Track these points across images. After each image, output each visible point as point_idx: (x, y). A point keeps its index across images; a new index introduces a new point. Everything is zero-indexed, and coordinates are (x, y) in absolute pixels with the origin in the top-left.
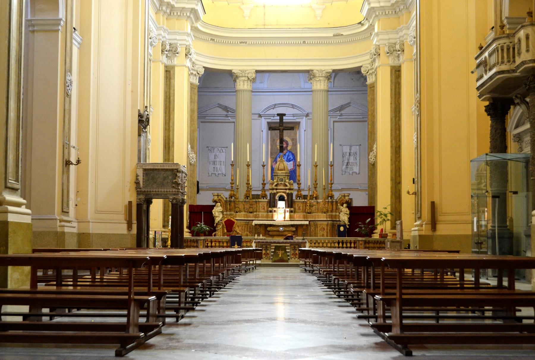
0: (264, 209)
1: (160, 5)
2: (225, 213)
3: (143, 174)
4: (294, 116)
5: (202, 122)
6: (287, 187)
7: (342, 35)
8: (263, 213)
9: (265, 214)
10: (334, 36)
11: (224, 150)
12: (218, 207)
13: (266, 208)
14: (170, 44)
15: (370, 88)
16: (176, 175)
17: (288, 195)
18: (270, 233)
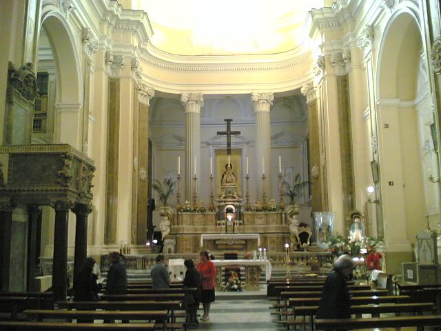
1: (104, 15)
3: (10, 161)
6: (235, 200)
8: (211, 226)
13: (214, 222)
14: (115, 57)
15: (311, 106)
16: (64, 162)
18: (219, 247)
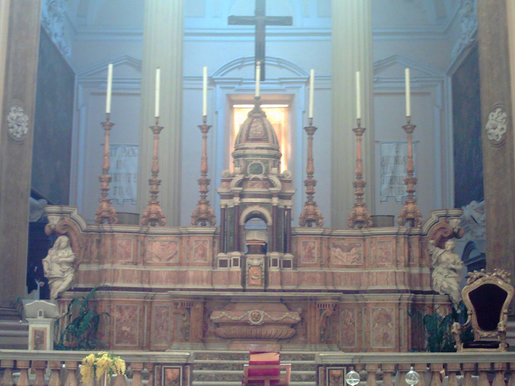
0: (203, 255)
2: (83, 268)
4: (281, 83)
5: (93, 94)
9: (206, 270)
11: (137, 151)
12: (59, 248)
13: (209, 253)
17: (277, 212)
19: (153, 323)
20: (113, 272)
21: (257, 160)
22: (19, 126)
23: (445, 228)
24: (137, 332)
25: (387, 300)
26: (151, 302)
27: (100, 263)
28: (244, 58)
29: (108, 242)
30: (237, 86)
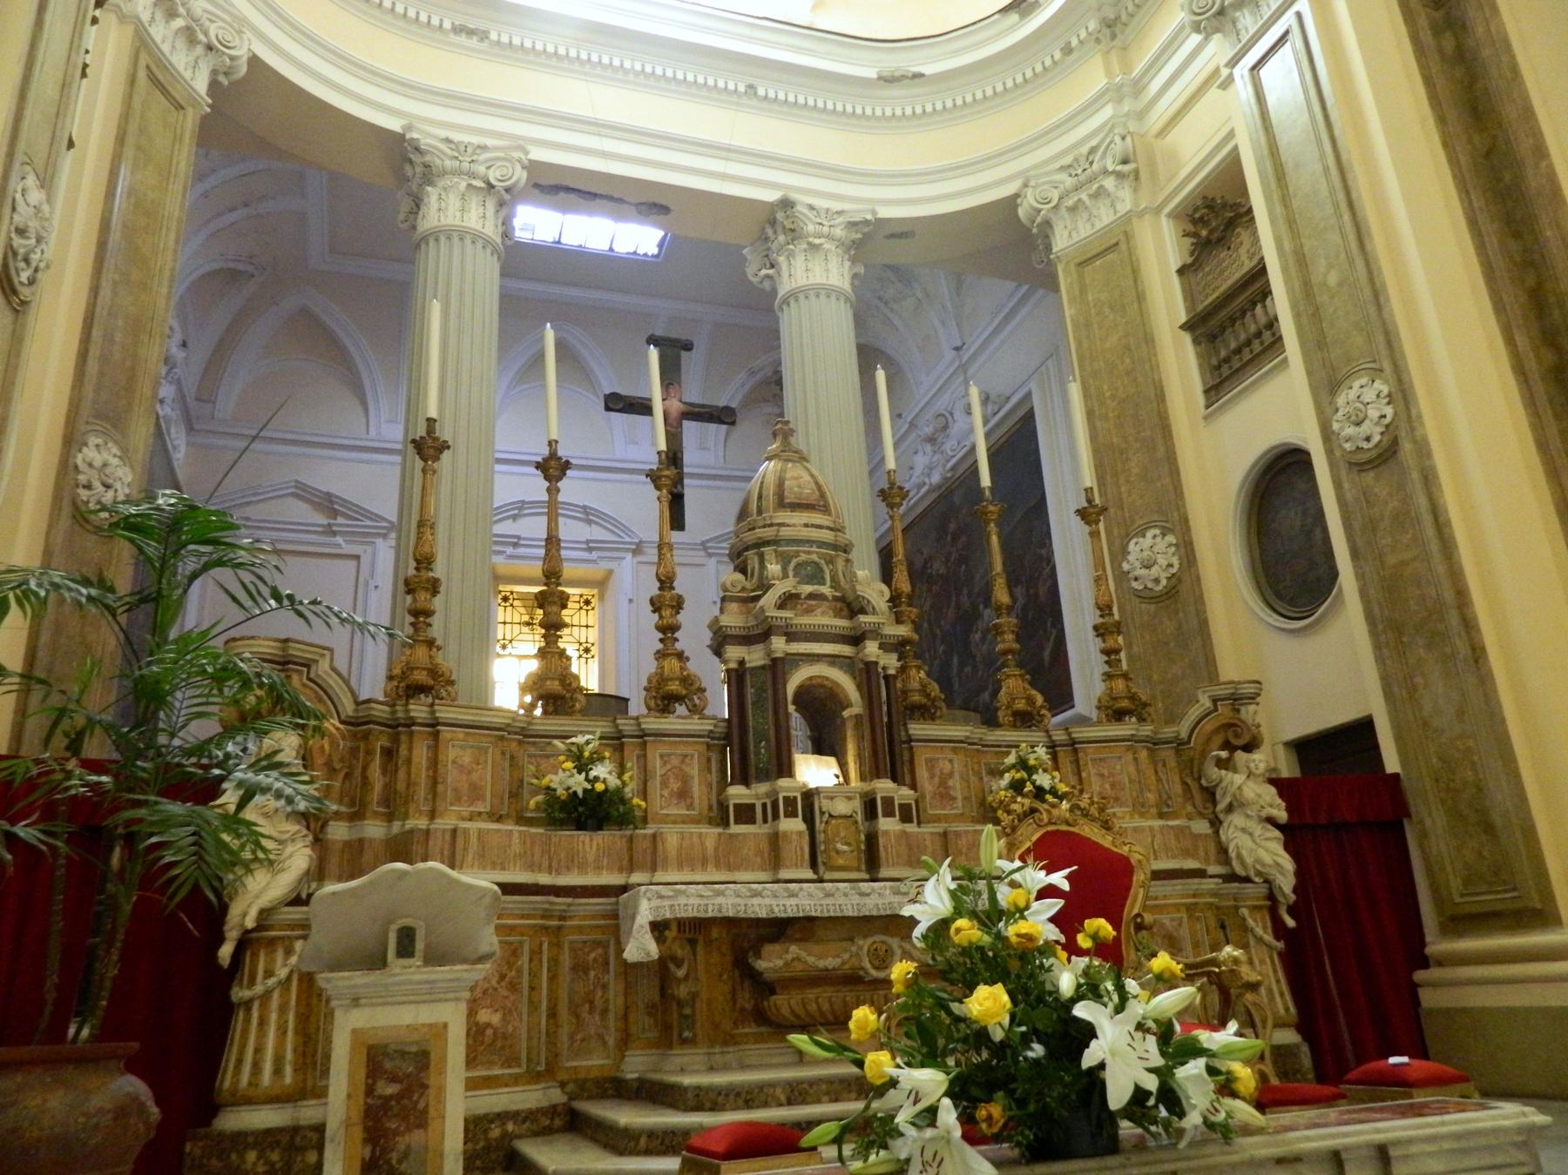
0: (683, 794)
2: (338, 832)
4: (590, 550)
7: (922, 75)
10: (880, 78)
19: (563, 995)
20: (448, 837)
21: (809, 553)
22: (107, 486)
23: (1234, 725)
24: (520, 1026)
25: (1165, 897)
26: (559, 928)
27: (389, 818)
28: (523, 502)
29: (421, 754)
30: (510, 550)
